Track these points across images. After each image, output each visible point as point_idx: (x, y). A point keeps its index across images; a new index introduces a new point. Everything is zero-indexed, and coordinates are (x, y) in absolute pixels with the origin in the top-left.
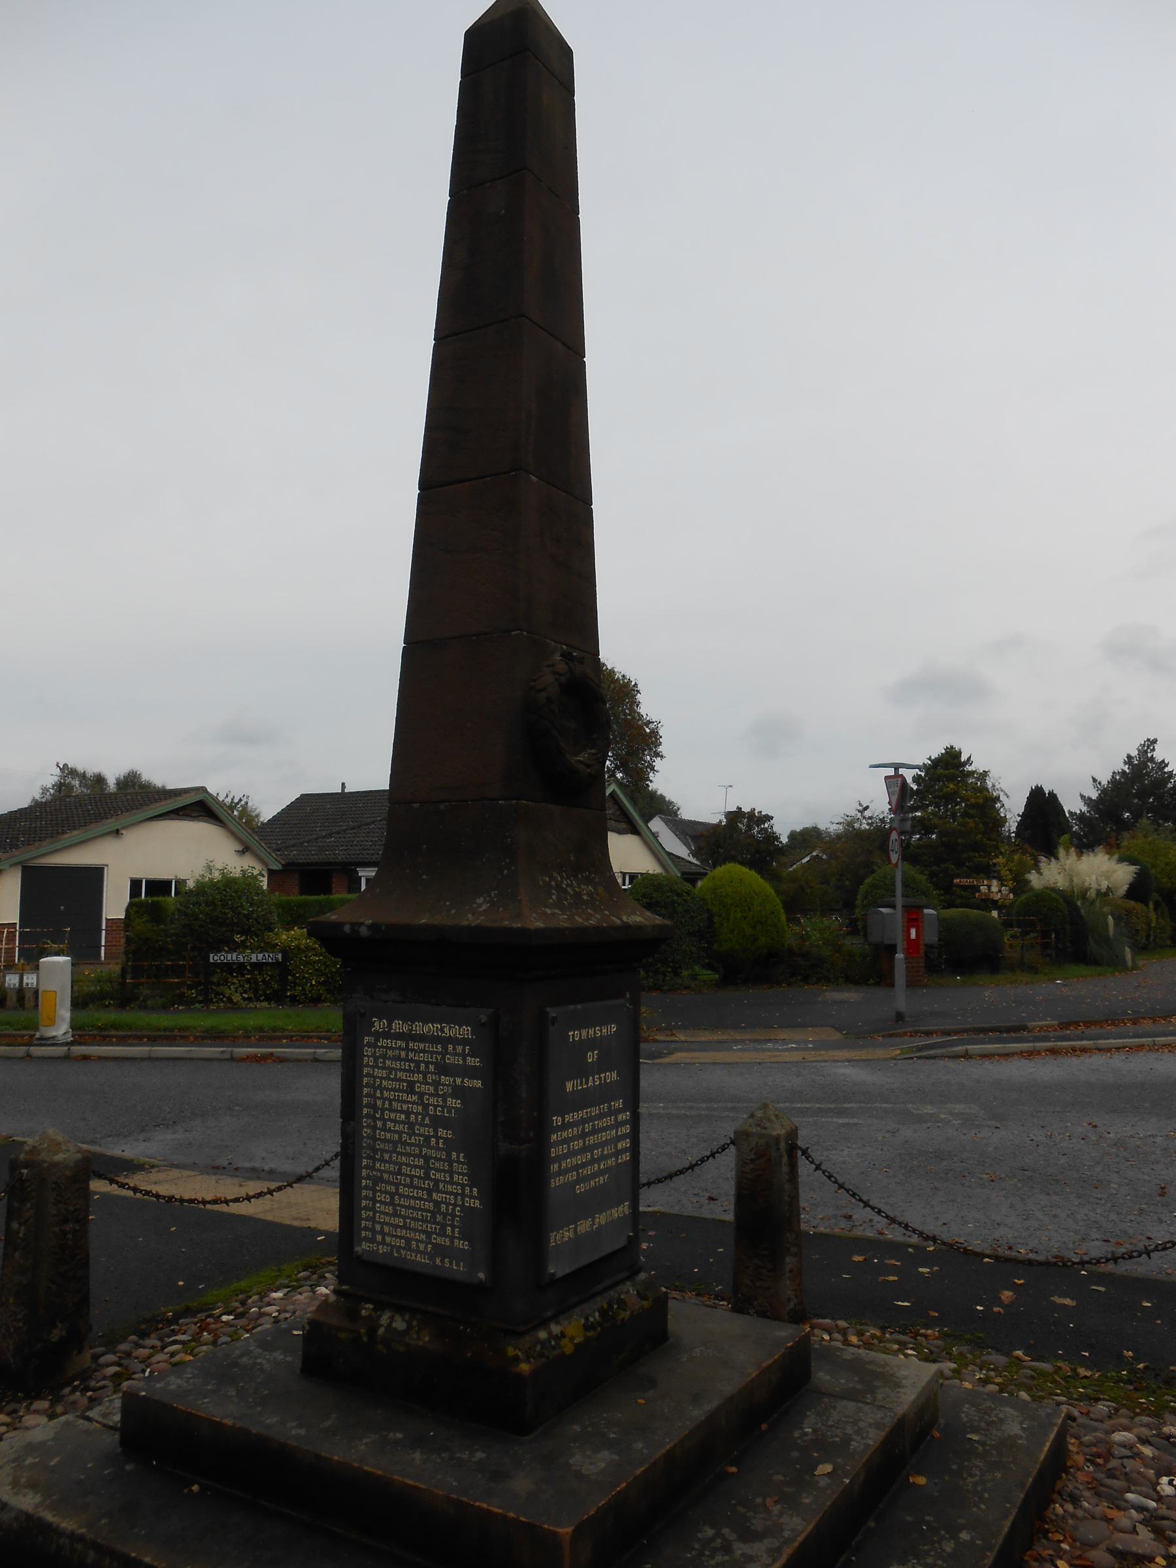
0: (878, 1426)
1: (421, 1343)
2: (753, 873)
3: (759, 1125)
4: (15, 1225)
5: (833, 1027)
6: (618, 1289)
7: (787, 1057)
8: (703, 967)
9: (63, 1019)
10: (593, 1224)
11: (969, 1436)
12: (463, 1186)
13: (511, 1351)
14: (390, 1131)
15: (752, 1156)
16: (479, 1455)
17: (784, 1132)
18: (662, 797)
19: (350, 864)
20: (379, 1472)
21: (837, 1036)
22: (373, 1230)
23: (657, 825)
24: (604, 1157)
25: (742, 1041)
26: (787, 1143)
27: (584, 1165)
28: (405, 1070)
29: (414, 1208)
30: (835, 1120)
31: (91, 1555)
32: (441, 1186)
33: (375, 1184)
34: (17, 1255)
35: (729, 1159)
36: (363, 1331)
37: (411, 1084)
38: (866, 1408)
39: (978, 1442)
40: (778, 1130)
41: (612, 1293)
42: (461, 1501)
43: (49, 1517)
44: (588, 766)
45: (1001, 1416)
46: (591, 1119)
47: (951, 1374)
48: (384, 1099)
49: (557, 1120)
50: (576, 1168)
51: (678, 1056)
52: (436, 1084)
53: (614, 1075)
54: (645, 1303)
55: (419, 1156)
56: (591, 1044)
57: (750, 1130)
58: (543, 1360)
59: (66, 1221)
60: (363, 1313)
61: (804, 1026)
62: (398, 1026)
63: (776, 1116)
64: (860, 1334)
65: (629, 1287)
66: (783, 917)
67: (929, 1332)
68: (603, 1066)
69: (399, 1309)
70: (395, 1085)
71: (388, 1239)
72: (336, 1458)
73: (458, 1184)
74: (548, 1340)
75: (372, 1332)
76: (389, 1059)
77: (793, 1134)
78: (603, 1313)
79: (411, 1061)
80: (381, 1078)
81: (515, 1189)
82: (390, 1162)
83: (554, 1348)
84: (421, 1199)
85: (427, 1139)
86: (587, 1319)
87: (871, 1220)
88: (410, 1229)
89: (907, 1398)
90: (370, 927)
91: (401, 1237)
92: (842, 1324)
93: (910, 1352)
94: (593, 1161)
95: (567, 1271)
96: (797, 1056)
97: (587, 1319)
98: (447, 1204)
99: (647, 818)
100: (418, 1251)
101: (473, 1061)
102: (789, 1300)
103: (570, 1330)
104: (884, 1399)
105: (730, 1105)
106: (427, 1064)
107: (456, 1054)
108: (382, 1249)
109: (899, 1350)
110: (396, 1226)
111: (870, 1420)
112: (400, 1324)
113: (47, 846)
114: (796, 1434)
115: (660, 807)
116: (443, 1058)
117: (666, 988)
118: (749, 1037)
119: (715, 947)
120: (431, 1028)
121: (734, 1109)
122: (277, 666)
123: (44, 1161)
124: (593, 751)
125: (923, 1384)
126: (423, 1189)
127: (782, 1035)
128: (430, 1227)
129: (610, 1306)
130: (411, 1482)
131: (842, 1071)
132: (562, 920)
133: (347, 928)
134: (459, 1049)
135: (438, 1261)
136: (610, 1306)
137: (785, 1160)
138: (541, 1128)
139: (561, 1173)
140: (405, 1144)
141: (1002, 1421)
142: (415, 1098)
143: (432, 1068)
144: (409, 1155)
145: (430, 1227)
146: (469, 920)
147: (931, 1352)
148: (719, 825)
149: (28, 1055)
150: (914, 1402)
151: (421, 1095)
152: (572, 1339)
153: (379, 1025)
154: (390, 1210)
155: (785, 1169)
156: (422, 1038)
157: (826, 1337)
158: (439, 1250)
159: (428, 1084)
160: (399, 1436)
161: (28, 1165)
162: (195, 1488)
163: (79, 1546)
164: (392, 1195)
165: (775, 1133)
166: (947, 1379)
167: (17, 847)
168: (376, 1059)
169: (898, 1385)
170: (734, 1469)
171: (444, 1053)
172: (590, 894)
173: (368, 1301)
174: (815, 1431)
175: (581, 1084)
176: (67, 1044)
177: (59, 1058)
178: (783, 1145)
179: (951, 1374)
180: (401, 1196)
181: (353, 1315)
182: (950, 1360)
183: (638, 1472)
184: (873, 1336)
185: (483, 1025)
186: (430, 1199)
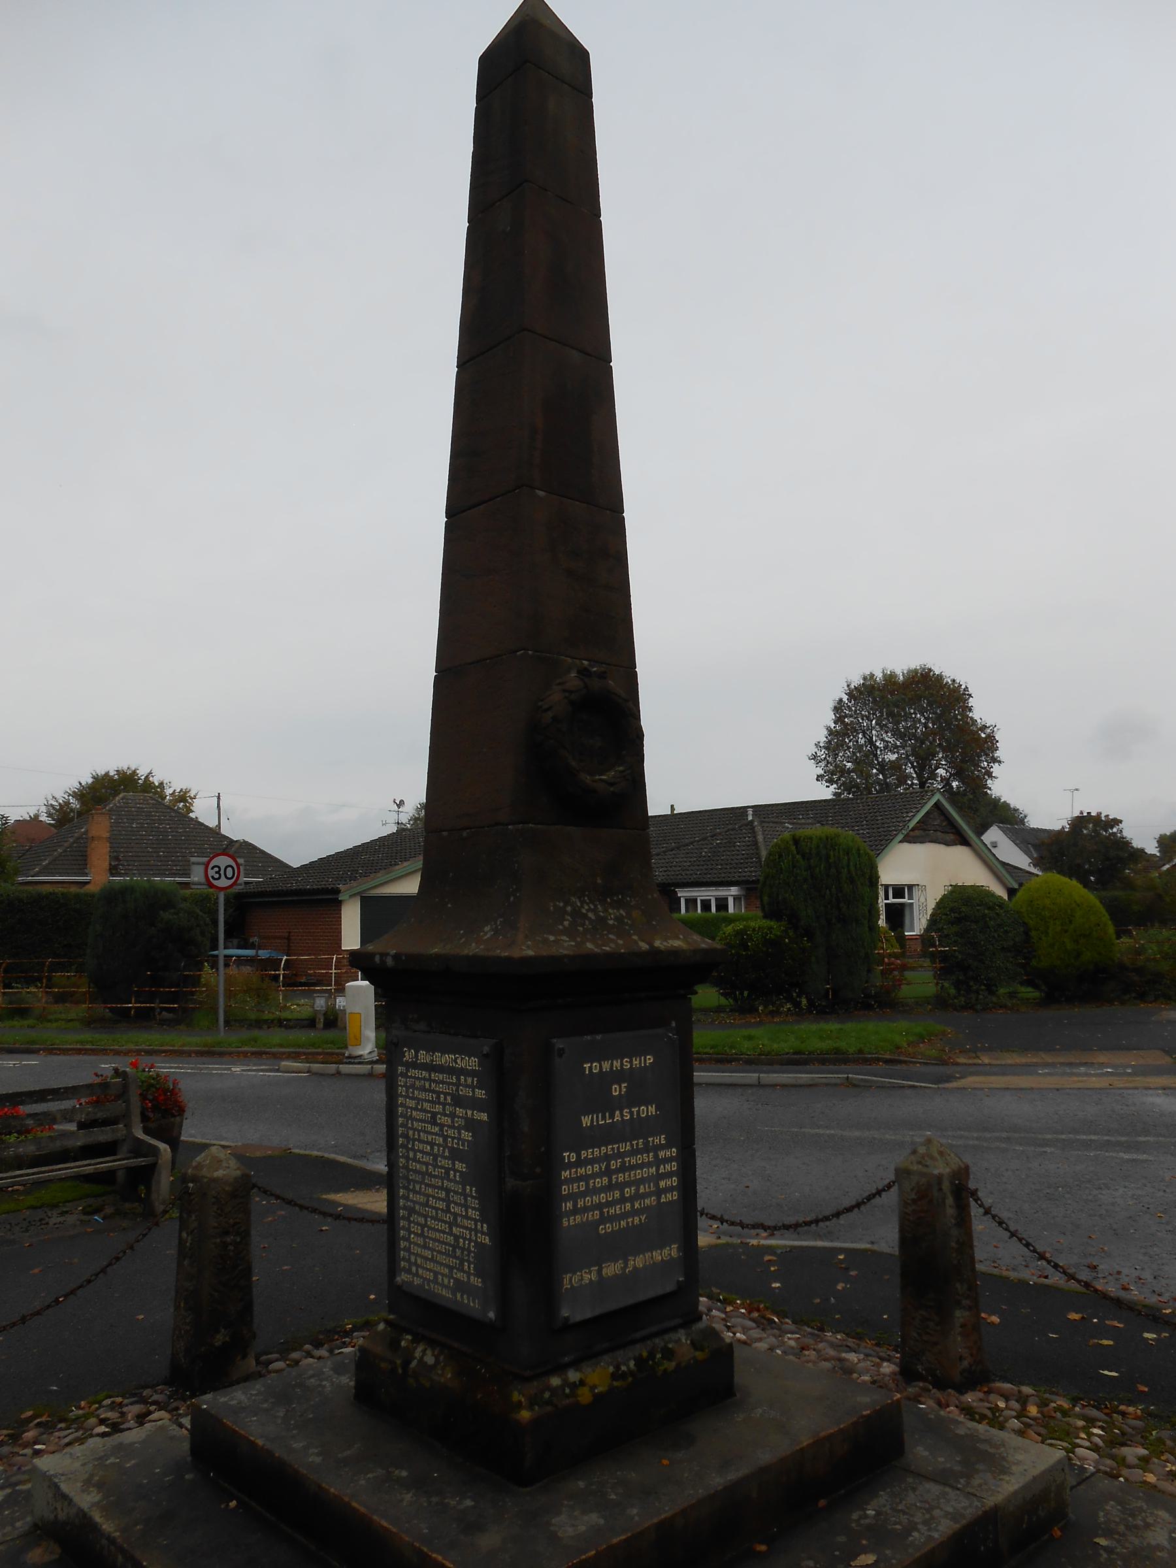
0: (954, 1517)
1: (442, 1380)
2: (1074, 882)
3: (919, 1163)
4: (184, 1235)
5: (1164, 1051)
6: (666, 1337)
7: (1095, 1082)
8: (1022, 984)
9: (368, 1039)
10: (626, 1266)
11: (1097, 1540)
12: (476, 1221)
13: (516, 1396)
14: (419, 1162)
15: (913, 1196)
16: (469, 1503)
17: (948, 1170)
18: (1006, 805)
19: (670, 885)
20: (363, 1510)
21: (1167, 1060)
22: (409, 1261)
23: (993, 835)
24: (638, 1196)
25: (1053, 1065)
26: (952, 1183)
27: (609, 1204)
28: (429, 1101)
29: (439, 1241)
30: (1122, 1154)
31: (120, 1558)
32: (459, 1219)
33: (409, 1215)
34: (186, 1262)
35: (891, 1198)
36: (399, 1362)
37: (434, 1115)
38: (952, 1493)
39: (1105, 1548)
40: (940, 1168)
41: (657, 1341)
42: (422, 1551)
43: (97, 1517)
44: (612, 784)
45: (1150, 1520)
46: (620, 1155)
47: (1136, 1461)
48: (415, 1130)
49: (569, 1156)
50: (599, 1206)
51: (970, 1081)
52: (453, 1115)
53: (652, 1110)
54: (699, 1355)
55: (442, 1188)
56: (619, 1076)
57: (911, 1168)
58: (549, 1408)
59: (227, 1233)
60: (403, 1343)
61: (1128, 1048)
62: (423, 1057)
63: (941, 1153)
64: (1043, 1404)
65: (682, 1336)
66: (1111, 930)
67: (1131, 1409)
68: (632, 1099)
69: (432, 1343)
70: (421, 1115)
71: (420, 1271)
72: (332, 1490)
73: (472, 1219)
74: (562, 1387)
75: (406, 1363)
76: (417, 1089)
77: (962, 1174)
78: (640, 1361)
79: (433, 1091)
80: (412, 1108)
81: (524, 1227)
82: (419, 1193)
83: (567, 1396)
84: (444, 1232)
85: (447, 1171)
86: (618, 1367)
87: (1119, 1273)
88: (438, 1262)
89: (1004, 1489)
90: (396, 957)
91: (430, 1270)
92: (1027, 1390)
93: (1096, 1431)
94: (623, 1200)
95: (588, 1315)
96: (1102, 1083)
97: (618, 1367)
98: (465, 1239)
99: (981, 829)
100: (443, 1285)
101: (480, 1094)
102: (961, 1358)
103: (596, 1377)
104: (980, 1485)
105: (1004, 1135)
106: (446, 1094)
107: (467, 1086)
108: (417, 1281)
109: (1084, 1428)
110: (426, 1259)
111: (951, 1510)
112: (430, 1359)
113: (382, 877)
114: (855, 1516)
115: (1006, 816)
116: (457, 1090)
117: (979, 1007)
118: (1062, 1060)
119: (1034, 963)
120: (447, 1059)
121: (1008, 1140)
122: (298, 704)
123: (204, 1177)
124: (621, 768)
125: (1036, 1472)
126: (445, 1222)
127: (1102, 1058)
128: (452, 1262)
129: (652, 1355)
130: (385, 1524)
131: (1150, 1099)
132: (565, 946)
133: (377, 959)
134: (469, 1080)
135: (459, 1296)
136: (652, 1355)
137: (950, 1201)
138: (548, 1166)
139: (575, 1211)
140: (430, 1175)
141: (1148, 1526)
142: (437, 1129)
143: (449, 1098)
144: (435, 1187)
145: (452, 1262)
146: (473, 949)
147: (1123, 1434)
148: (1062, 831)
149: (339, 1073)
150: (1016, 1493)
151: (442, 1126)
152: (593, 1387)
153: (409, 1055)
154: (420, 1241)
155: (950, 1211)
156: (440, 1069)
157: (1002, 1404)
158: (460, 1286)
159: (446, 1115)
160: (404, 1474)
161: (194, 1179)
162: (233, 1504)
163: (112, 1548)
164: (423, 1226)
165: (936, 1172)
166: (1129, 1467)
167: (355, 879)
168: (407, 1088)
169: (1005, 1471)
170: (763, 1548)
171: (458, 1084)
172: (619, 919)
173: (408, 1332)
174: (878, 1513)
175: (604, 1118)
176: (372, 1062)
177: (364, 1075)
178: (946, 1185)
179: (1136, 1461)
180: (430, 1228)
181: (394, 1345)
182: (1142, 1445)
183: (615, 1541)
184: (1059, 1409)
185: (486, 1056)
186: (451, 1233)
